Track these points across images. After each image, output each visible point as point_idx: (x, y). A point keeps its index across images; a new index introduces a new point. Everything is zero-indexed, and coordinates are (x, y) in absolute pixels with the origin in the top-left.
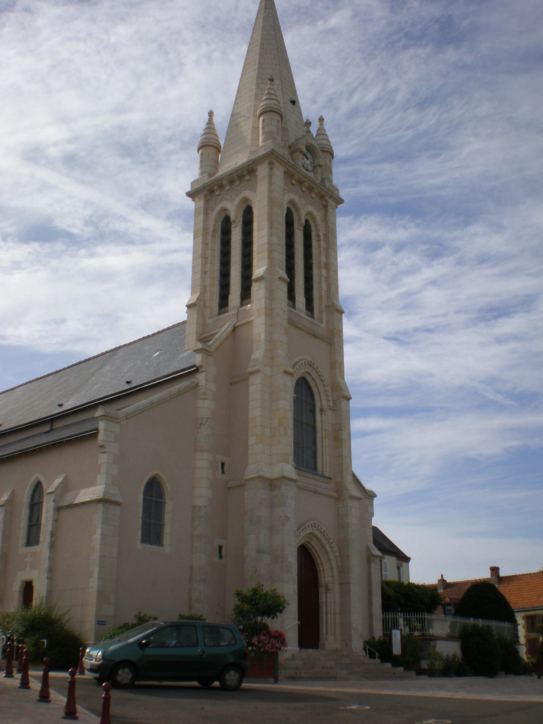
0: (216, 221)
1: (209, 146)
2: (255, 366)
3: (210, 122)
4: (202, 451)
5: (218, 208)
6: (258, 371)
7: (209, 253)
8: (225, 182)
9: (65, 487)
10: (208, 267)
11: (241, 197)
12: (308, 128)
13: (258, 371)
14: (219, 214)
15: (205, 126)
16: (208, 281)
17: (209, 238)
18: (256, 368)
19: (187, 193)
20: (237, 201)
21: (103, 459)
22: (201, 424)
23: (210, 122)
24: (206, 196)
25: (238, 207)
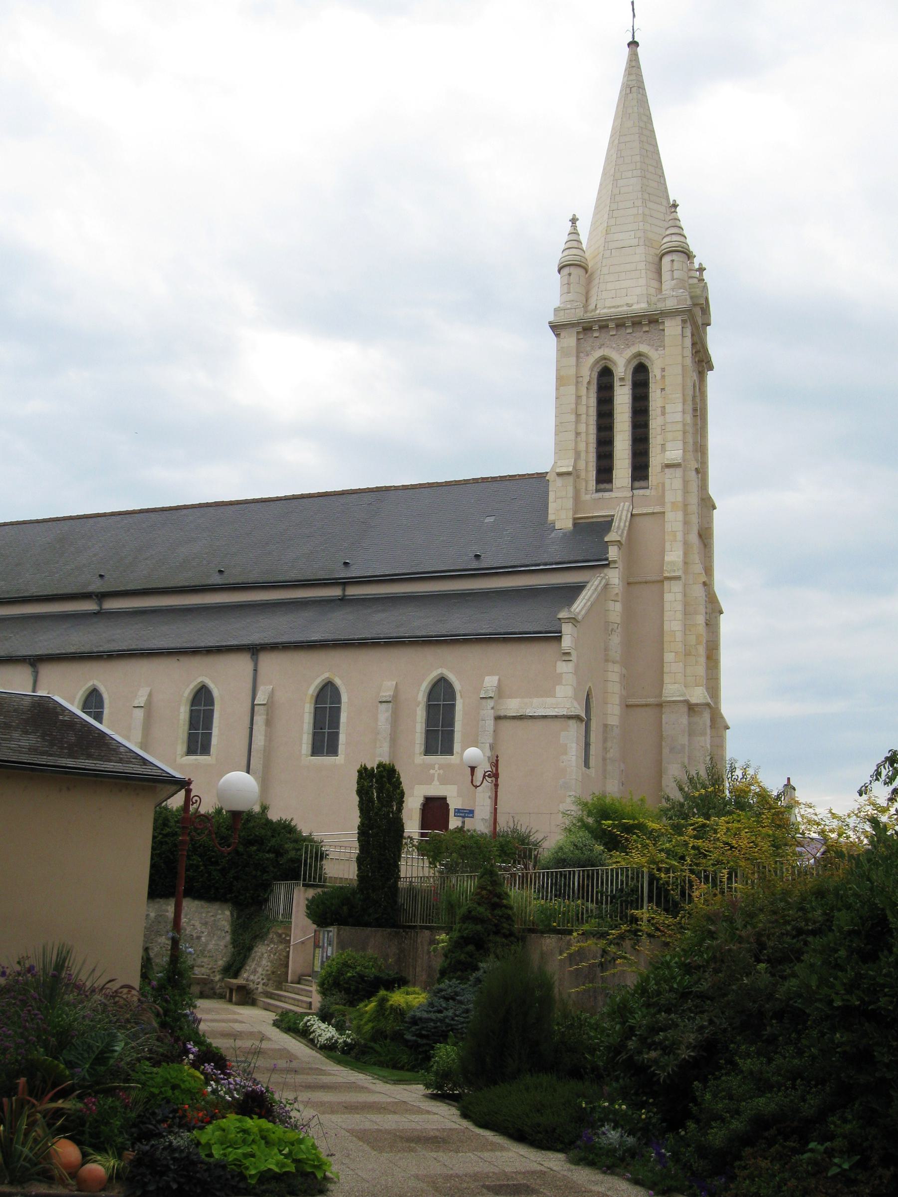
0: (592, 369)
1: (575, 267)
2: (674, 571)
3: (574, 232)
4: (613, 662)
5: (598, 354)
6: (678, 578)
7: (582, 410)
8: (612, 325)
9: (501, 693)
10: (582, 428)
11: (634, 350)
12: (701, 274)
13: (678, 578)
14: (597, 362)
15: (566, 238)
16: (582, 446)
17: (583, 391)
18: (676, 574)
19: (550, 323)
20: (630, 352)
21: (563, 667)
22: (612, 630)
23: (574, 232)
24: (578, 333)
25: (629, 361)
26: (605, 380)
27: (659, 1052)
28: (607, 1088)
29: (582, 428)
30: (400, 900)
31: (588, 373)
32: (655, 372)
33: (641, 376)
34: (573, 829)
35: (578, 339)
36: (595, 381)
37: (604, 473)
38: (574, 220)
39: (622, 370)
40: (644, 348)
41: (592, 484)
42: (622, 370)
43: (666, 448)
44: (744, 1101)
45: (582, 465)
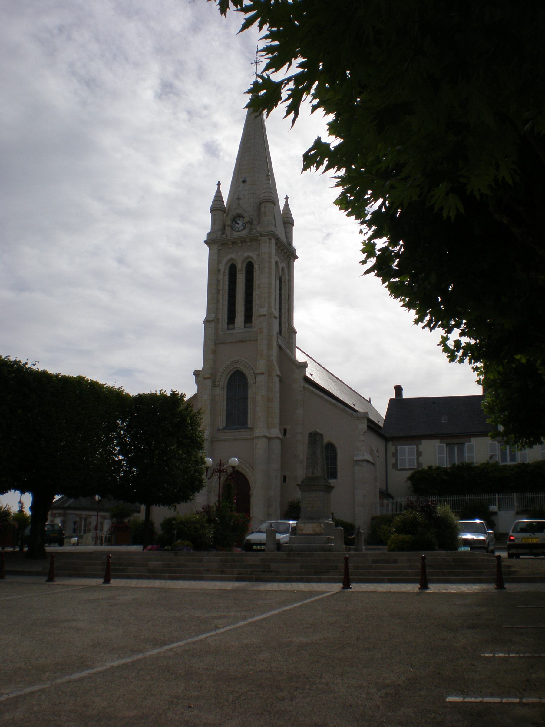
5: (229, 257)
14: (229, 261)
23: (219, 192)
26: (233, 270)
27: (48, 673)
28: (506, 414)
29: (221, 277)
30: (137, 504)
31: (224, 267)
32: (256, 266)
33: (250, 268)
34: (220, 248)
35: (219, 250)
36: (227, 272)
37: (231, 320)
38: (219, 184)
39: (241, 267)
40: (250, 254)
41: (226, 325)
42: (241, 267)
43: (260, 308)
44: (279, 546)
45: (220, 316)
